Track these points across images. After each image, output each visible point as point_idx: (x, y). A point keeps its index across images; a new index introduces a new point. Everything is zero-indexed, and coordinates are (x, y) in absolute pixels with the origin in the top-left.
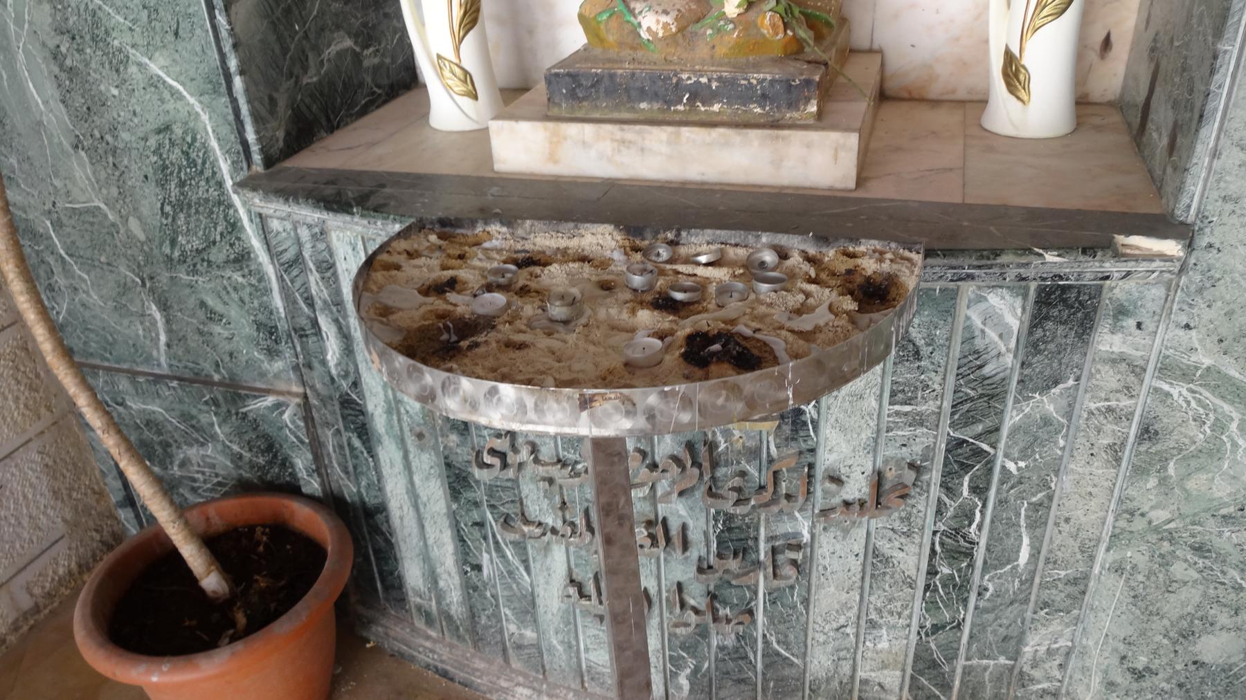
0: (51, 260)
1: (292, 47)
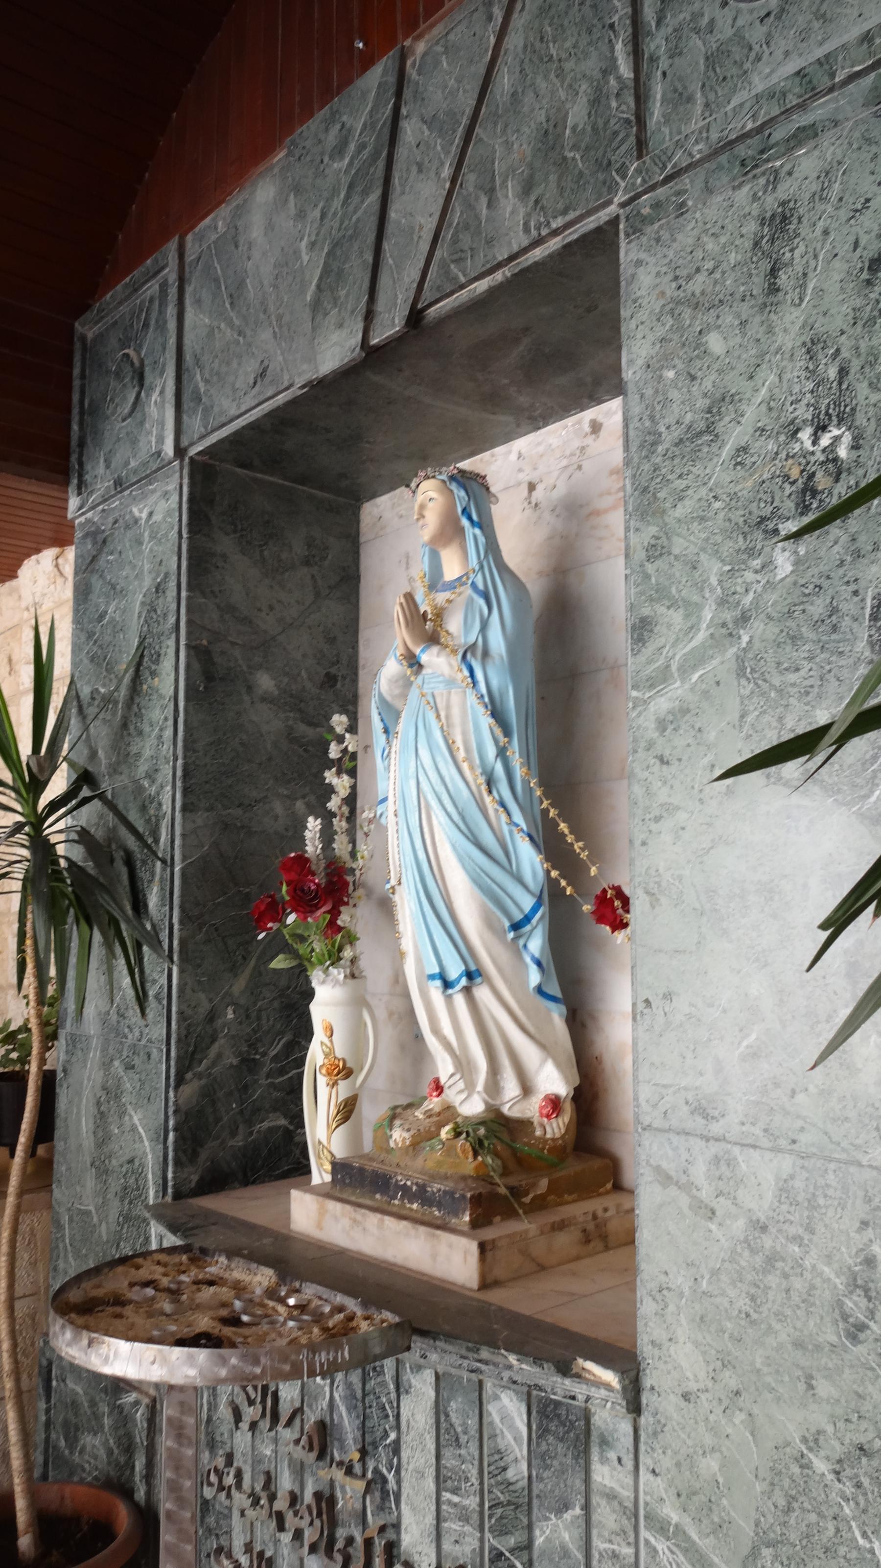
0: (61, 1245)
1: (225, 1119)
